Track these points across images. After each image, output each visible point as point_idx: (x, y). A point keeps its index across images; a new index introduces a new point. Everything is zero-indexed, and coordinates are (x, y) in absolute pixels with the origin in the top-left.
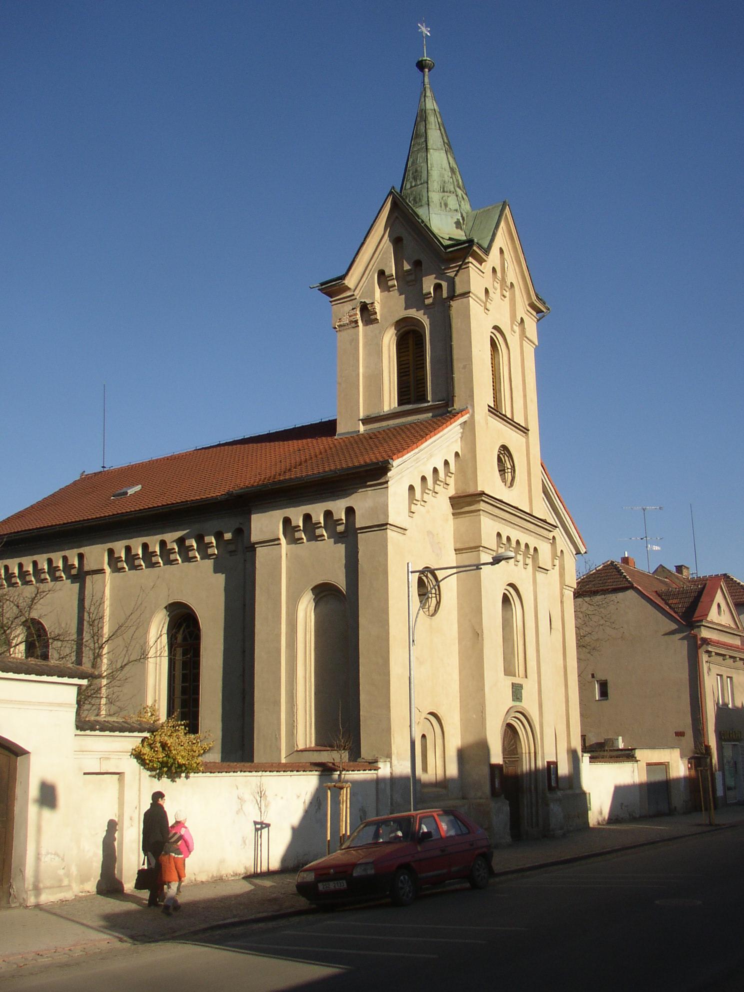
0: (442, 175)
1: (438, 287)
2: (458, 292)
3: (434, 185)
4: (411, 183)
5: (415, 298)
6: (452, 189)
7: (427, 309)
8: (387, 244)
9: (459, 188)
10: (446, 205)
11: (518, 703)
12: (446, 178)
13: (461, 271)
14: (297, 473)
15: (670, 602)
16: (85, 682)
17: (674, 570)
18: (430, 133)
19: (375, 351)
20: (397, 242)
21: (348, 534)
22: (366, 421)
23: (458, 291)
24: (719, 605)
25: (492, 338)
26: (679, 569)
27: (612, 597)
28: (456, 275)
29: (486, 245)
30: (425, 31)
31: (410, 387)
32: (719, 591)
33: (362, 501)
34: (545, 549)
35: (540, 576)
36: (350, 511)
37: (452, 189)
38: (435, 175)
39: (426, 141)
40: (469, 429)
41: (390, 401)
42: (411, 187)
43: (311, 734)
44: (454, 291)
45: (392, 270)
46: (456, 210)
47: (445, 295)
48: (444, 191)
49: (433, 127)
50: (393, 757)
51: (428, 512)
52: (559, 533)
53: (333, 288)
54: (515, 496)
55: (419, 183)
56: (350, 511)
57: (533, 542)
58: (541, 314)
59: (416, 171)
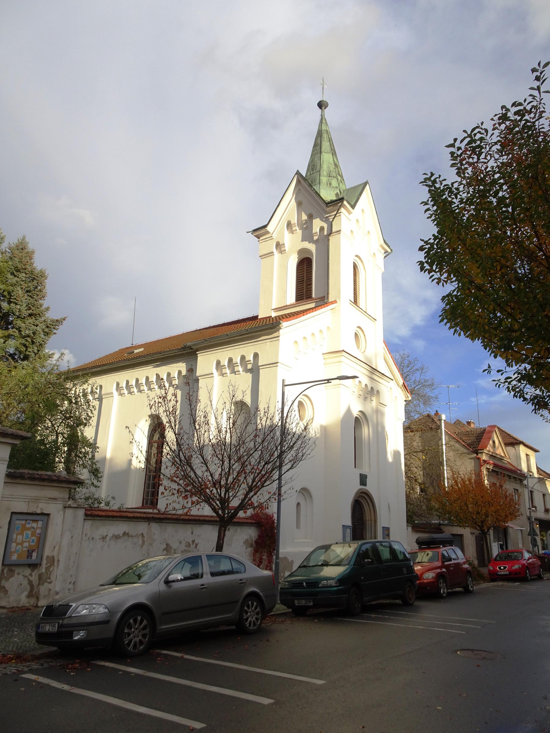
0: (329, 167)
1: (322, 229)
2: (334, 230)
3: (324, 172)
5: (307, 236)
6: (335, 175)
7: (316, 242)
8: (293, 204)
9: (340, 175)
10: (330, 184)
12: (331, 169)
13: (336, 218)
14: (509, 537)
15: (463, 439)
16: (17, 442)
17: (466, 423)
18: (323, 143)
19: (284, 266)
20: (299, 204)
21: (254, 371)
22: (276, 310)
23: (334, 230)
24: (494, 442)
25: (354, 263)
26: (469, 423)
28: (333, 220)
29: (353, 203)
31: (304, 291)
32: (494, 433)
36: (256, 356)
37: (335, 175)
38: (325, 167)
39: (321, 148)
41: (291, 298)
42: (310, 174)
44: (331, 230)
45: (294, 221)
46: (337, 187)
47: (325, 233)
48: (329, 176)
49: (326, 140)
53: (260, 232)
56: (256, 356)
58: (387, 254)
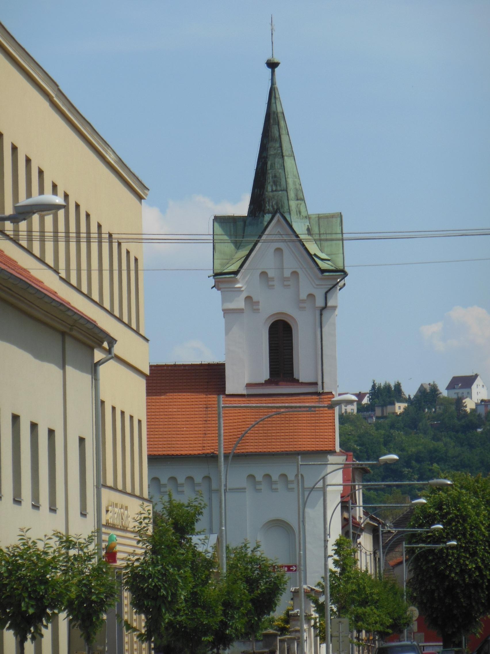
10: (300, 212)
42: (272, 191)
48: (297, 200)
59: (275, 176)
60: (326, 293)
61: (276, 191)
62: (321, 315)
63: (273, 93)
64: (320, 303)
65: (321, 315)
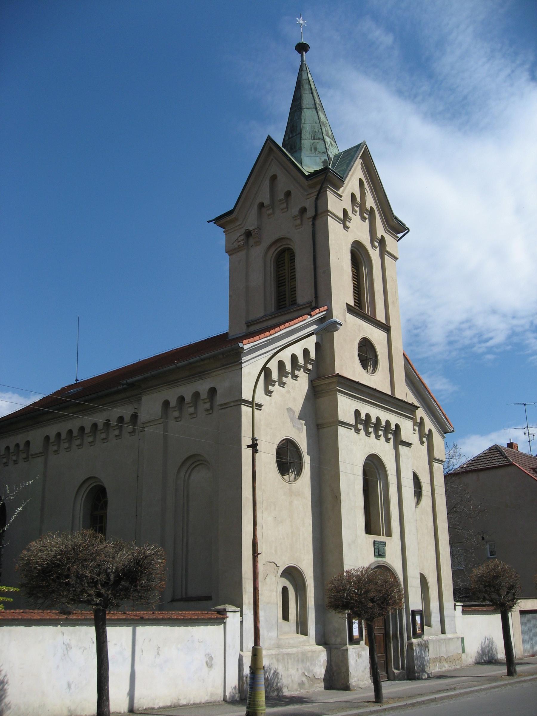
4: (289, 135)
6: (321, 137)
9: (329, 137)
10: (316, 149)
11: (380, 559)
27: (430, 390)
30: (301, 21)
33: (218, 381)
34: (408, 430)
35: (403, 449)
40: (327, 328)
43: (367, 302)
46: (324, 153)
48: (314, 139)
50: (244, 607)
51: (289, 392)
52: (421, 413)
54: (378, 381)
55: (294, 135)
57: (394, 419)
60: (317, 199)
61: (292, 137)
62: (313, 224)
63: (302, 68)
64: (310, 213)
65: (313, 224)
